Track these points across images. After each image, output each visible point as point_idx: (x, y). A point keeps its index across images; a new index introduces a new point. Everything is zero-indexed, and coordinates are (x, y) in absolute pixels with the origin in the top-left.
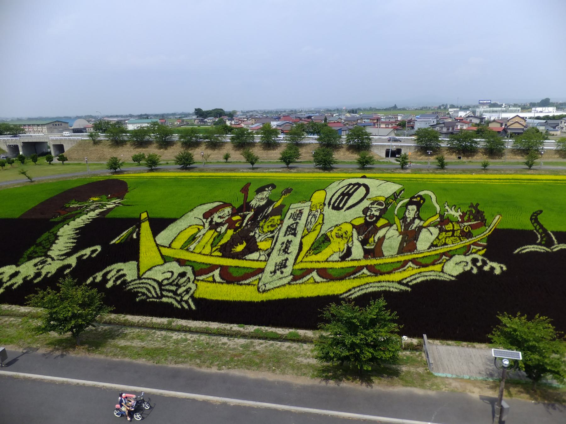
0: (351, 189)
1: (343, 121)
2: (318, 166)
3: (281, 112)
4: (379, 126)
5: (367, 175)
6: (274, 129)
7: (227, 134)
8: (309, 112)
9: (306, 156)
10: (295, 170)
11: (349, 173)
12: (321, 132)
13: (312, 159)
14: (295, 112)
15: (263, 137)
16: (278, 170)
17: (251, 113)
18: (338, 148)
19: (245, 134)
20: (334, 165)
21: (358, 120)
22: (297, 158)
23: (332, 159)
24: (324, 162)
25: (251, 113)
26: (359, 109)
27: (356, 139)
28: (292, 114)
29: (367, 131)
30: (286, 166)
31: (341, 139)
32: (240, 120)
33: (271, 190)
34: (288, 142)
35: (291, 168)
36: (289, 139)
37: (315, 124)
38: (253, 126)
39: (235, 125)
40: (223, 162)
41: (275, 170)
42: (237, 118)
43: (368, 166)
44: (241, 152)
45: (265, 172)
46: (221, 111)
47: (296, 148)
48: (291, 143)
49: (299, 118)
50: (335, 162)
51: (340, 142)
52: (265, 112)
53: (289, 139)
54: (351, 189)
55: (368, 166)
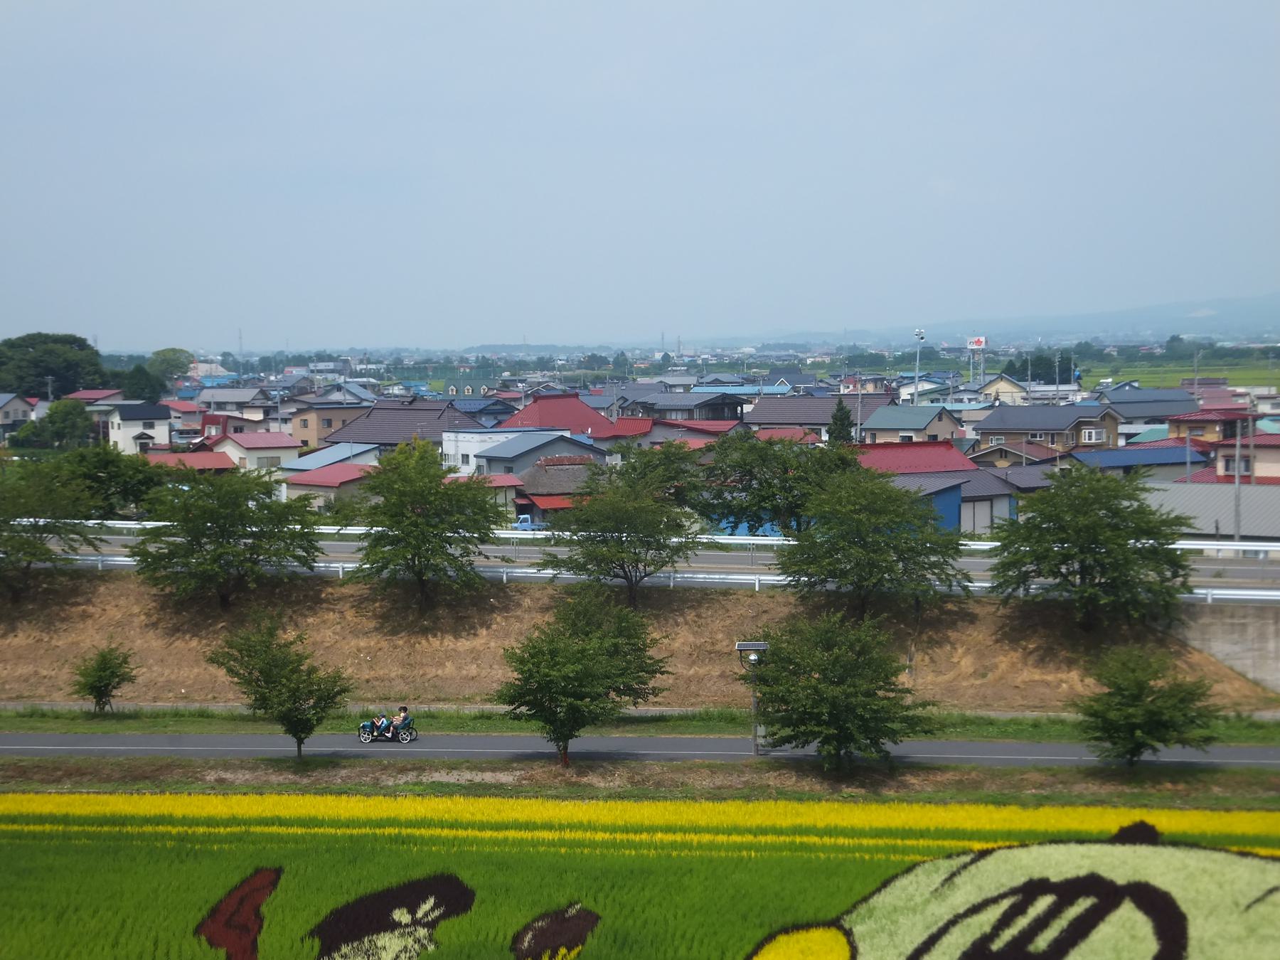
0: (1041, 923)
1: (970, 434)
2: (788, 751)
3: (519, 366)
4: (1238, 469)
5: (1163, 820)
6: (469, 484)
7: (110, 514)
8: (720, 366)
9: (700, 680)
10: (618, 781)
11: (1024, 805)
12: (811, 508)
13: (745, 696)
14: (622, 367)
15: (378, 540)
16: (488, 777)
17: (298, 372)
18: (936, 624)
19: (245, 519)
20: (910, 747)
21: (1078, 426)
22: (629, 691)
23: (896, 703)
24: (835, 719)
25: (298, 372)
26: (1091, 353)
27: (1066, 558)
28: (598, 380)
29: (1152, 501)
30: (551, 748)
31: (962, 562)
32: (213, 421)
33: (431, 925)
34: (566, 575)
35: (591, 761)
36: (577, 554)
37: (764, 454)
38: (311, 462)
39: (173, 449)
40: (73, 718)
41: (466, 776)
42: (194, 405)
43: (1170, 754)
44: (217, 643)
45: (392, 793)
46: (74, 354)
47: (621, 619)
48: (585, 588)
49: (648, 408)
50: (916, 725)
51: (947, 580)
52: (397, 368)
53: (577, 554)
54: (1041, 923)
55: (1170, 754)
